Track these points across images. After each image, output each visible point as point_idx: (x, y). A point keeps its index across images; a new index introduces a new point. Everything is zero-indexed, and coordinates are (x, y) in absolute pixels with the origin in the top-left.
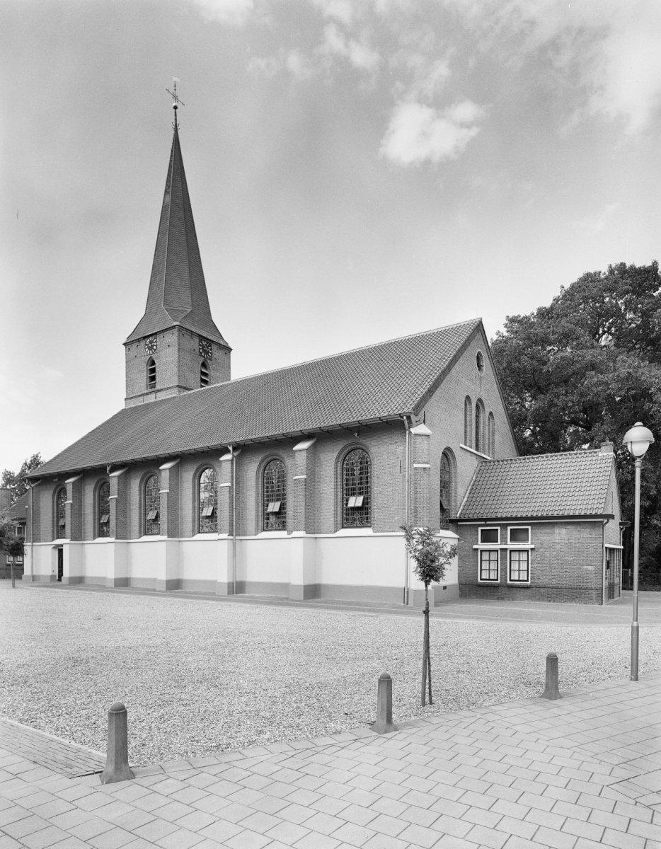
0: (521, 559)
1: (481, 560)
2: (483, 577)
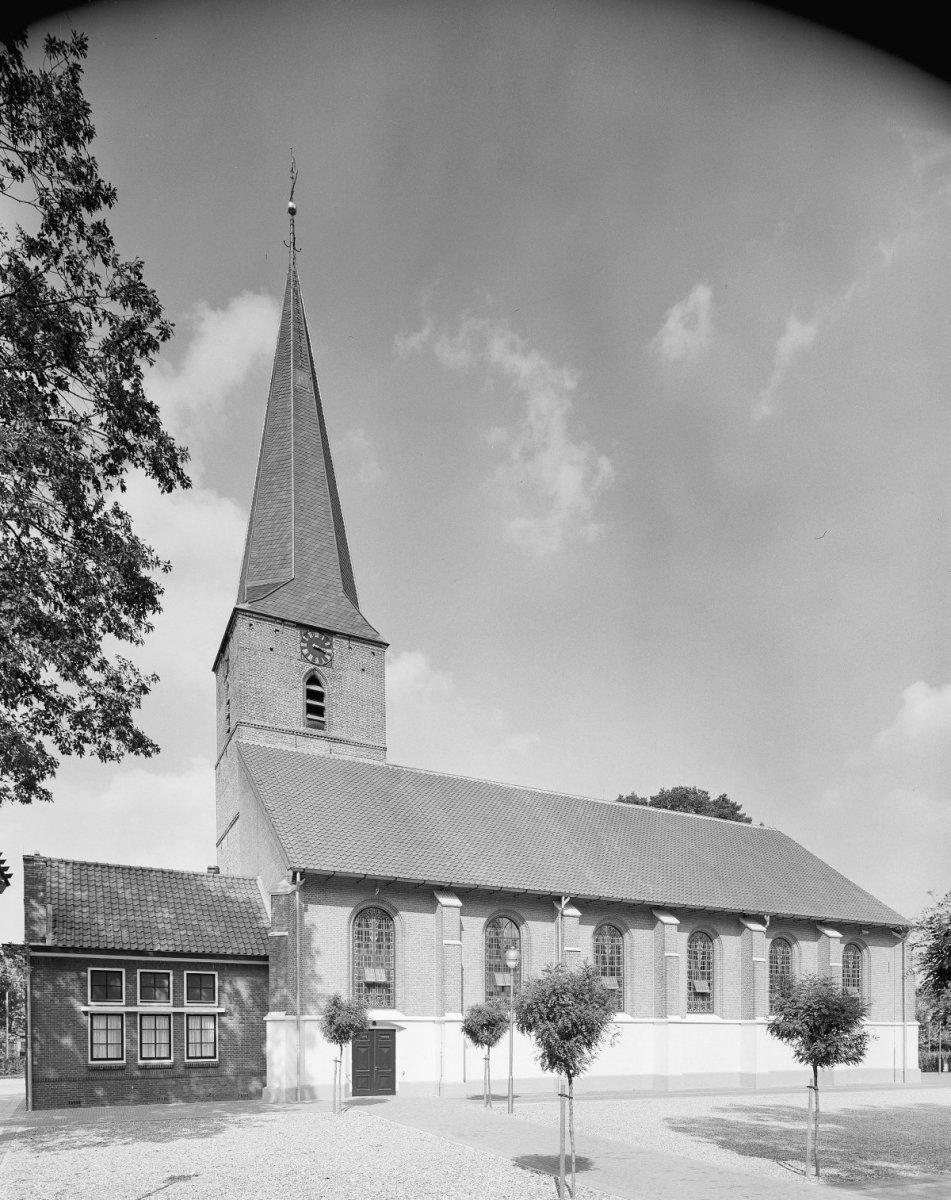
0: (198, 1032)
2: (212, 1054)
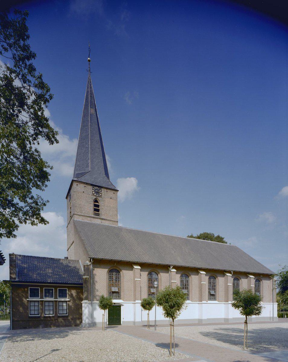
0: (50, 305)
1: (45, 306)
2: (60, 313)
